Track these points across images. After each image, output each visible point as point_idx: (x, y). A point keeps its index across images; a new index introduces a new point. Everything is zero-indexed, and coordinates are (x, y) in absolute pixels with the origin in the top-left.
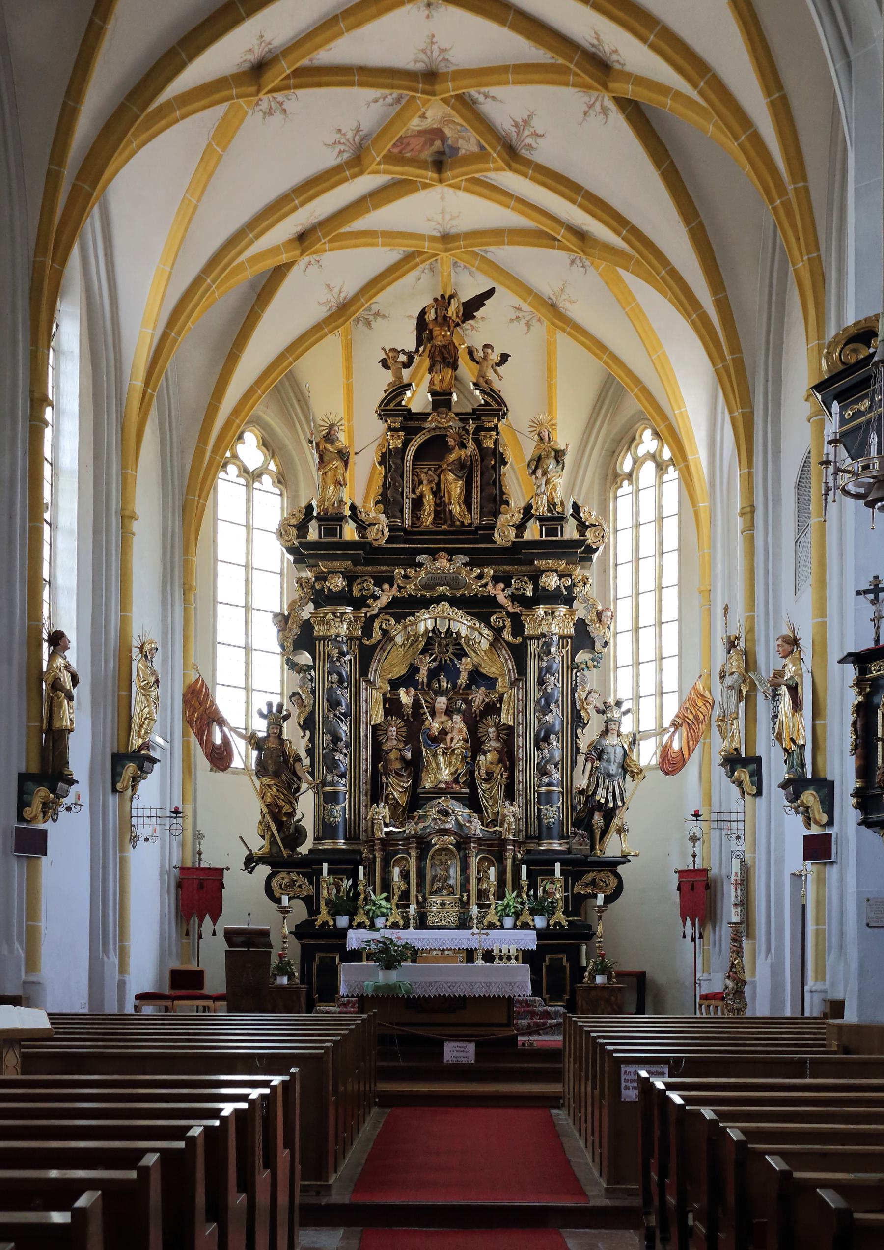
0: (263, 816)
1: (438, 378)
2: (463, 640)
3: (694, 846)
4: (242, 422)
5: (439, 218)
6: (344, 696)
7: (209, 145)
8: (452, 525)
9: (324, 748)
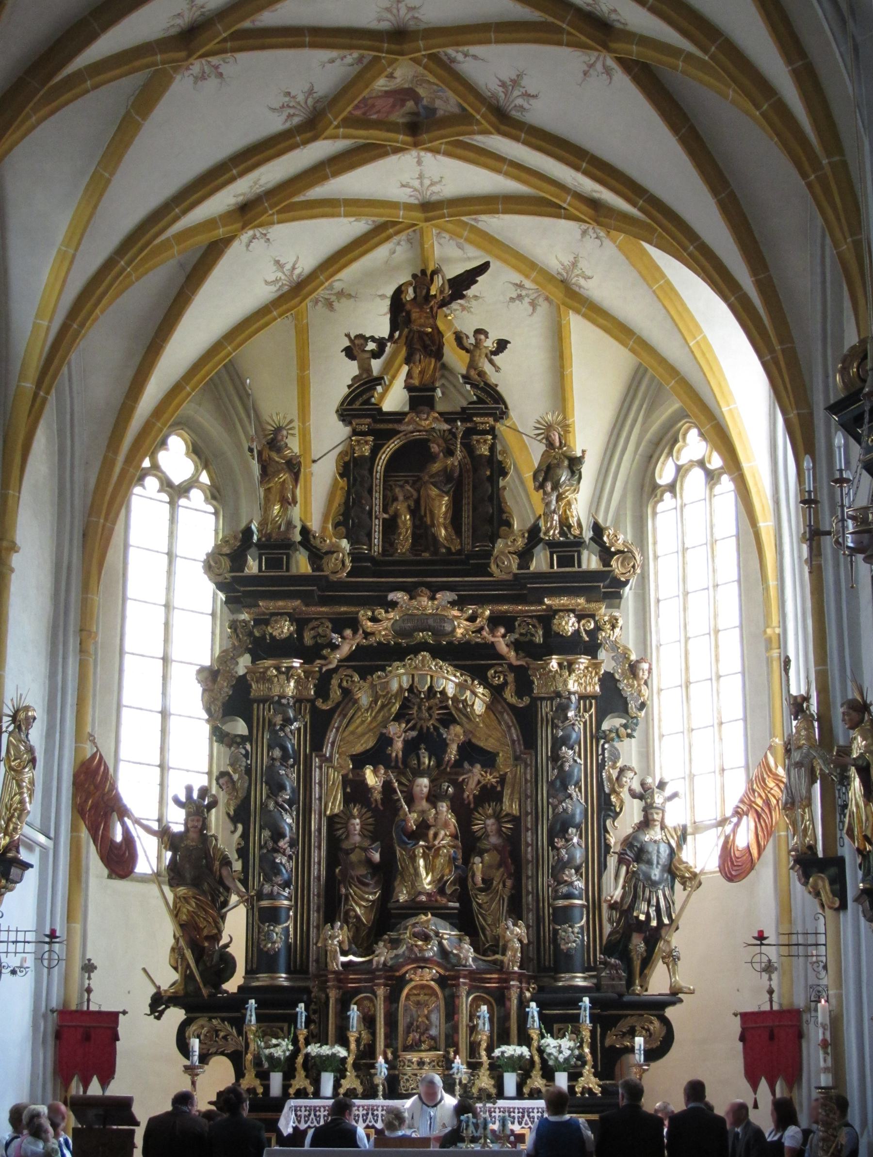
0: (177, 940)
1: (416, 371)
2: (450, 702)
3: (770, 979)
4: (164, 425)
5: (416, 183)
6: (290, 777)
7: (128, 113)
8: (436, 552)
9: (261, 847)
